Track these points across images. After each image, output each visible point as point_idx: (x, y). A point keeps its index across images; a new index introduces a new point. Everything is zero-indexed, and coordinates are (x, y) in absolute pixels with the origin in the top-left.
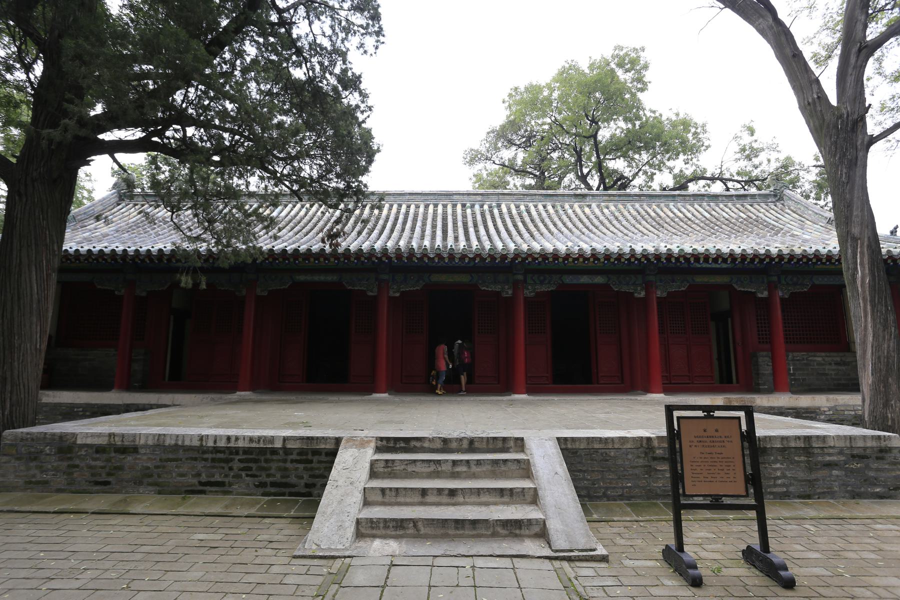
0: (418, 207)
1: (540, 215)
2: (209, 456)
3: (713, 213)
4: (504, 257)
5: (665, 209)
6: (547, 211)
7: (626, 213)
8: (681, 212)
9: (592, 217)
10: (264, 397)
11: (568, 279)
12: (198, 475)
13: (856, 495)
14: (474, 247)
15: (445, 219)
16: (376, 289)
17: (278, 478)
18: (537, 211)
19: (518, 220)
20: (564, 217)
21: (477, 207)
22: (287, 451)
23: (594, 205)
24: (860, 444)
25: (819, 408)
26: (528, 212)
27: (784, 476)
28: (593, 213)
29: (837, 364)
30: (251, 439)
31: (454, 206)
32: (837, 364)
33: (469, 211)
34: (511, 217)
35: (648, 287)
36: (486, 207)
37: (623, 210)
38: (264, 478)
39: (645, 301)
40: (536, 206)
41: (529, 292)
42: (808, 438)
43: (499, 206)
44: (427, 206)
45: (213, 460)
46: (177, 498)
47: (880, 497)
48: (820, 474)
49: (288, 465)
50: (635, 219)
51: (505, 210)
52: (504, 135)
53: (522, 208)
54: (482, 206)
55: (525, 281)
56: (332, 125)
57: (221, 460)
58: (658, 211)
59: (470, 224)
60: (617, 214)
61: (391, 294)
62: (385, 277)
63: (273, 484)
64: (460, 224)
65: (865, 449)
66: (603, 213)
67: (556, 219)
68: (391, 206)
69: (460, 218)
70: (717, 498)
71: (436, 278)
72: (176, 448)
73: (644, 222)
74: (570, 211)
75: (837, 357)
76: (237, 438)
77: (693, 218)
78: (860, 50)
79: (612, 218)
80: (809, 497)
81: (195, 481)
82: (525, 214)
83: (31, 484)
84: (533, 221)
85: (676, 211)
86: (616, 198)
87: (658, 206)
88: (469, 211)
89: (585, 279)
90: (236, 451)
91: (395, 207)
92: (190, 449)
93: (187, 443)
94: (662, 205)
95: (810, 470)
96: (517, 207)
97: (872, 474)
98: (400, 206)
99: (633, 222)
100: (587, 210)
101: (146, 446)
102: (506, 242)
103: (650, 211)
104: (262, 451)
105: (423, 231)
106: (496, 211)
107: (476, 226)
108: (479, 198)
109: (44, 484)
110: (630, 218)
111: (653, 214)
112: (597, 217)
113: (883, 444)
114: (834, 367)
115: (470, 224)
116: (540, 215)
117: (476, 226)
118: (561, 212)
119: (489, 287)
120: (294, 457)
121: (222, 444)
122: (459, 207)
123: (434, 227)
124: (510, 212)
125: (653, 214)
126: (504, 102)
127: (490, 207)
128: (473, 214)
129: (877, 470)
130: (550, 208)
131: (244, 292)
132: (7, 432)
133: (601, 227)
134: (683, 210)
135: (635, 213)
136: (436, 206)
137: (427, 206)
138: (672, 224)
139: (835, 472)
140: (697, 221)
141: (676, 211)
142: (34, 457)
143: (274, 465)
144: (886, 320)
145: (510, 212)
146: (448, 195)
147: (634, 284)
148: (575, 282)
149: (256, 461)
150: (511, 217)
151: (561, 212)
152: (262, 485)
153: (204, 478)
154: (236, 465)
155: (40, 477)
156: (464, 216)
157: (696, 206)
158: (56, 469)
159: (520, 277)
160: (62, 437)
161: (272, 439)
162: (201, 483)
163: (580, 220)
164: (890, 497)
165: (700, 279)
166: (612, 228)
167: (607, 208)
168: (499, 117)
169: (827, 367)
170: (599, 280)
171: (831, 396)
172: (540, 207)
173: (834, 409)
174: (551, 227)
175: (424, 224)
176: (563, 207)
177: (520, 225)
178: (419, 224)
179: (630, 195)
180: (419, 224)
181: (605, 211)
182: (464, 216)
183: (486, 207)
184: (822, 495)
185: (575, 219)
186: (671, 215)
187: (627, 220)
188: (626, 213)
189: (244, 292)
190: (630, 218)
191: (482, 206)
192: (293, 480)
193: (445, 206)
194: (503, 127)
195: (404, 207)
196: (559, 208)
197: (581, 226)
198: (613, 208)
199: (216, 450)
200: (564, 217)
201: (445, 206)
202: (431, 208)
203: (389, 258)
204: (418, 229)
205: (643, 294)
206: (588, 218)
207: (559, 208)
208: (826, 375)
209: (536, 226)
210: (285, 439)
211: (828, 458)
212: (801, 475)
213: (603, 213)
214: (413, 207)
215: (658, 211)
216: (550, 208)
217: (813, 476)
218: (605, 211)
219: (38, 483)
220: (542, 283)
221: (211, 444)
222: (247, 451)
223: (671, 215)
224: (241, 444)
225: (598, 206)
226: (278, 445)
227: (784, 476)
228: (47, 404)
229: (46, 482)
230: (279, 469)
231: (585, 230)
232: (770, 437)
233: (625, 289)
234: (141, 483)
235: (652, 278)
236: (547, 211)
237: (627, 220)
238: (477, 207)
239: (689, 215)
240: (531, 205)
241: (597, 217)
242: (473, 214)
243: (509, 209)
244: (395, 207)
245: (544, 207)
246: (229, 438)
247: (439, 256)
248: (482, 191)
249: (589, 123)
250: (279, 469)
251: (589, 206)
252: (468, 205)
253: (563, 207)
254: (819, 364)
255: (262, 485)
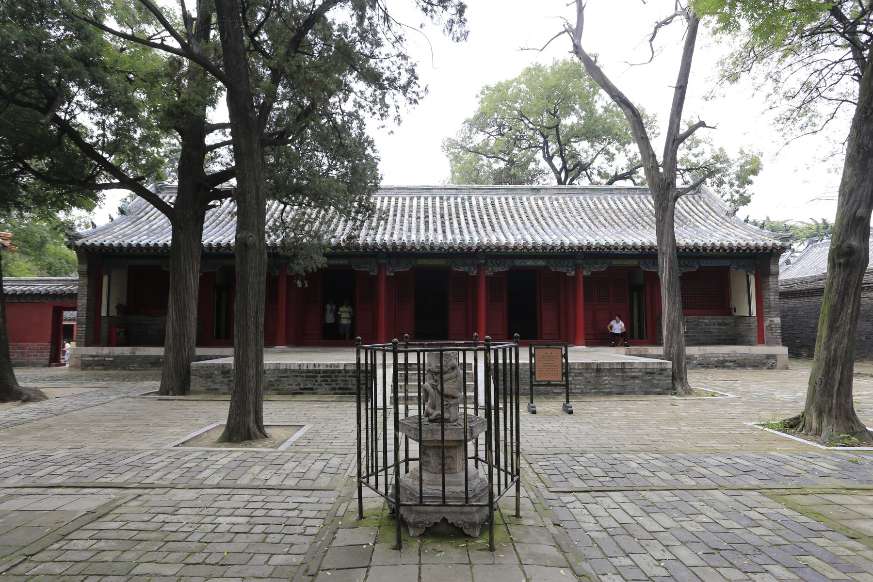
0: (404, 199)
1: (501, 207)
2: (304, 374)
3: (641, 205)
4: (470, 248)
5: (604, 202)
6: (507, 203)
7: (571, 205)
8: (615, 203)
9: (543, 209)
10: (290, 349)
11: (518, 263)
12: (299, 384)
13: (647, 393)
14: (449, 242)
15: (426, 211)
16: (376, 270)
17: (342, 385)
18: (500, 203)
19: (484, 212)
20: (521, 209)
21: (452, 200)
22: (346, 371)
23: (546, 198)
24: (651, 366)
25: (693, 356)
26: (493, 204)
27: (610, 383)
28: (545, 205)
29: (719, 324)
30: (327, 366)
31: (434, 198)
32: (719, 324)
33: (445, 204)
34: (479, 209)
35: (577, 268)
36: (459, 200)
37: (569, 202)
38: (334, 386)
39: (574, 278)
40: (499, 199)
41: (489, 273)
42: (623, 364)
43: (470, 198)
44: (411, 199)
45: (307, 377)
46: (291, 396)
47: (659, 394)
48: (628, 382)
49: (347, 378)
50: (577, 210)
51: (474, 203)
52: (479, 123)
53: (489, 200)
54: (456, 199)
55: (486, 264)
56: (359, 179)
57: (310, 377)
58: (597, 203)
59: (446, 217)
60: (564, 206)
61: (388, 273)
62: (383, 261)
63: (340, 389)
64: (438, 217)
65: (653, 369)
66: (552, 205)
67: (514, 212)
68: (383, 198)
69: (438, 210)
70: (549, 382)
71: (421, 262)
72: (286, 370)
73: (583, 214)
74: (526, 204)
75: (719, 319)
76: (319, 365)
77: (623, 210)
78: (674, 141)
79: (558, 210)
80: (622, 394)
81: (297, 388)
82: (490, 207)
83: (209, 391)
84: (495, 212)
85: (611, 203)
86: (565, 192)
87: (598, 198)
88: (445, 204)
89: (530, 263)
90: (319, 372)
91: (386, 199)
92: (294, 371)
93: (292, 368)
94: (602, 197)
95: (624, 380)
96: (484, 199)
97: (656, 382)
98: (390, 198)
99: (575, 213)
100: (540, 202)
101: (269, 370)
102: (472, 237)
103: (590, 203)
104: (333, 371)
105: (410, 223)
106: (467, 204)
107: (450, 218)
108: (454, 192)
109: (215, 390)
110: (573, 210)
111: (592, 206)
112: (547, 209)
113: (663, 366)
114: (717, 327)
115: (446, 217)
116: (501, 207)
117: (450, 218)
118: (519, 204)
119: (460, 268)
120: (350, 374)
121: (311, 368)
122: (438, 199)
123: (418, 218)
124: (478, 204)
125: (592, 206)
126: (477, 97)
127: (463, 199)
128: (449, 205)
129: (659, 380)
130: (510, 200)
131: (277, 272)
132: (192, 364)
133: (549, 220)
134: (618, 202)
135: (578, 205)
136: (419, 198)
137: (411, 199)
138: (606, 215)
139: (637, 381)
140: (626, 213)
141: (611, 203)
142: (209, 376)
143: (340, 379)
144: (674, 300)
145: (478, 204)
146: (429, 189)
147: (567, 266)
148: (523, 264)
149: (330, 377)
150: (479, 209)
151: (519, 204)
152: (334, 389)
153: (302, 386)
154: (319, 379)
155: (213, 386)
156: (442, 208)
157: (629, 198)
158: (222, 383)
159: (483, 261)
160: (223, 365)
161: (338, 365)
162: (301, 389)
163: (533, 213)
164: (664, 394)
165: (615, 262)
166: (557, 220)
167: (557, 200)
168: (472, 109)
169: (712, 327)
170: (541, 263)
171: (702, 347)
172: (503, 200)
173: (703, 356)
174: (509, 219)
175: (410, 216)
176: (521, 199)
177: (485, 217)
178: (406, 217)
179: (576, 189)
180: (406, 217)
181: (555, 203)
182: (442, 208)
183: (459, 200)
184: (629, 393)
185: (529, 212)
186: (607, 207)
187: (570, 212)
188: (571, 205)
189: (277, 272)
190: (573, 210)
191: (456, 199)
192: (350, 386)
193: (426, 199)
194: (477, 118)
195: (393, 199)
196: (518, 201)
197: (532, 218)
198: (561, 200)
199: (308, 371)
200: (521, 209)
201: (426, 199)
202: (415, 200)
203: (387, 249)
204: (406, 222)
205: (573, 273)
206: (539, 209)
207: (518, 201)
208: (711, 332)
209: (497, 218)
210: (345, 365)
211: (633, 374)
212: (619, 383)
213: (552, 205)
214: (400, 199)
215: (597, 203)
216: (510, 200)
217: (625, 383)
218: (555, 203)
219: (212, 390)
220: (498, 265)
221: (305, 368)
222: (325, 371)
223: (607, 207)
224: (321, 368)
225: (550, 199)
226: (342, 368)
227: (610, 383)
228: (139, 357)
229: (217, 389)
230: (343, 381)
231: (535, 222)
232: (603, 363)
233: (560, 269)
234: (268, 389)
235: (580, 262)
236: (507, 203)
237: (570, 212)
238: (452, 200)
239: (621, 207)
240: (495, 197)
241: (547, 209)
242: (449, 205)
243: (477, 201)
244: (386, 199)
245: (506, 199)
246: (315, 365)
247: (423, 248)
248: (456, 186)
249: (553, 116)
250: (343, 381)
251: (542, 199)
252: (445, 198)
253: (521, 199)
254: (706, 325)
255: (334, 389)
